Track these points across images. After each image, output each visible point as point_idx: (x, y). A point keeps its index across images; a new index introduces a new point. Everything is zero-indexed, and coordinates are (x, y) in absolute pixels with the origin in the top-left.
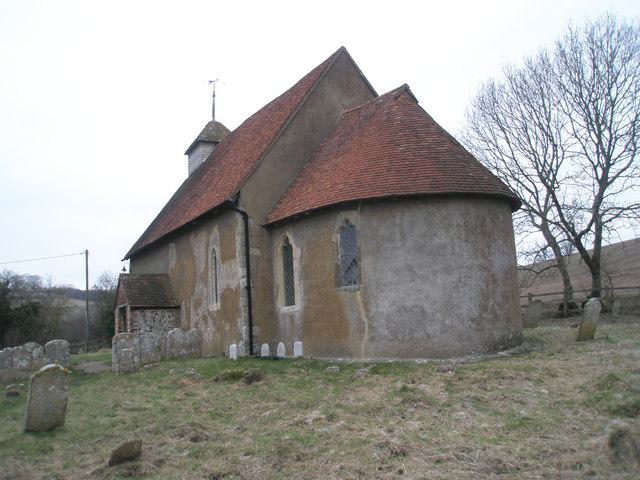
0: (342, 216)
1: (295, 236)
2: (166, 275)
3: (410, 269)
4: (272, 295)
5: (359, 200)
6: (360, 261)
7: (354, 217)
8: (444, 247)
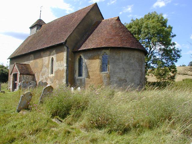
0: (104, 51)
1: (84, 56)
4: (74, 73)
5: (109, 47)
7: (108, 52)
8: (133, 63)
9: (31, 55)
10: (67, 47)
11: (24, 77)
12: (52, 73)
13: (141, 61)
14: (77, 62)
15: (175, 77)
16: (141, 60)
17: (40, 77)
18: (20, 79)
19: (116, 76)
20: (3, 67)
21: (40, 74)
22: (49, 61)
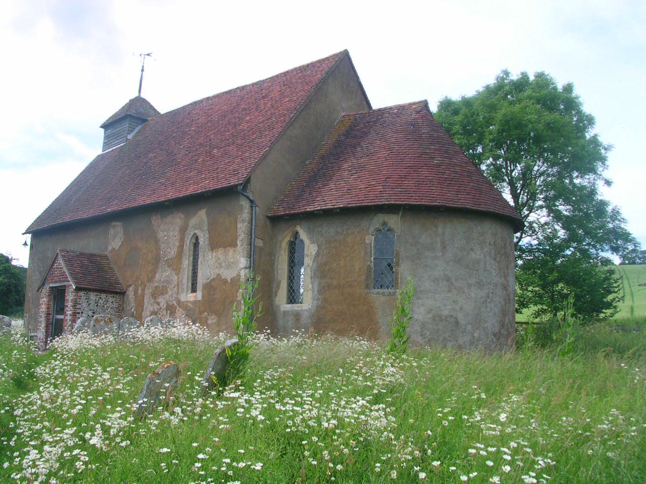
0: (378, 220)
1: (310, 232)
2: (106, 257)
3: (448, 279)
6: (398, 264)
7: (394, 221)
9: (114, 223)
10: (252, 201)
11: (88, 299)
12: (194, 290)
13: (505, 253)
14: (282, 252)
15: (596, 187)
16: (503, 252)
17: (146, 301)
18: (74, 306)
19: (423, 305)
20: (7, 260)
21: (146, 291)
22: (181, 247)
